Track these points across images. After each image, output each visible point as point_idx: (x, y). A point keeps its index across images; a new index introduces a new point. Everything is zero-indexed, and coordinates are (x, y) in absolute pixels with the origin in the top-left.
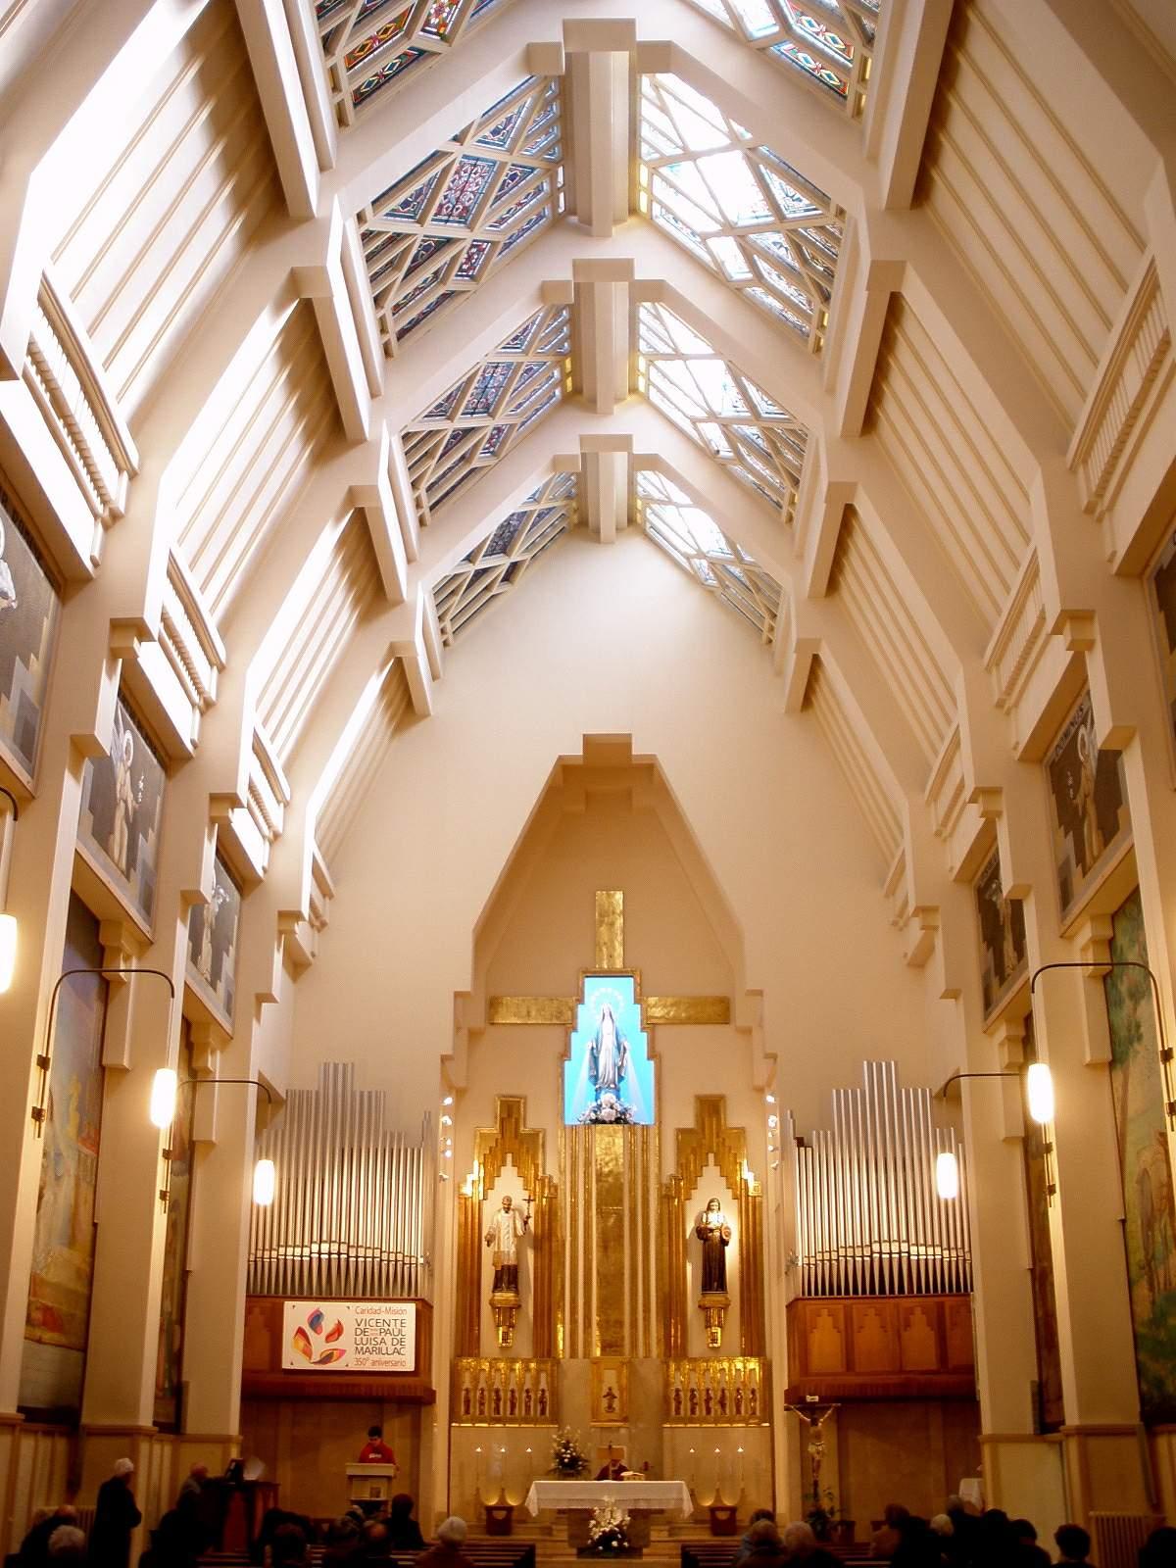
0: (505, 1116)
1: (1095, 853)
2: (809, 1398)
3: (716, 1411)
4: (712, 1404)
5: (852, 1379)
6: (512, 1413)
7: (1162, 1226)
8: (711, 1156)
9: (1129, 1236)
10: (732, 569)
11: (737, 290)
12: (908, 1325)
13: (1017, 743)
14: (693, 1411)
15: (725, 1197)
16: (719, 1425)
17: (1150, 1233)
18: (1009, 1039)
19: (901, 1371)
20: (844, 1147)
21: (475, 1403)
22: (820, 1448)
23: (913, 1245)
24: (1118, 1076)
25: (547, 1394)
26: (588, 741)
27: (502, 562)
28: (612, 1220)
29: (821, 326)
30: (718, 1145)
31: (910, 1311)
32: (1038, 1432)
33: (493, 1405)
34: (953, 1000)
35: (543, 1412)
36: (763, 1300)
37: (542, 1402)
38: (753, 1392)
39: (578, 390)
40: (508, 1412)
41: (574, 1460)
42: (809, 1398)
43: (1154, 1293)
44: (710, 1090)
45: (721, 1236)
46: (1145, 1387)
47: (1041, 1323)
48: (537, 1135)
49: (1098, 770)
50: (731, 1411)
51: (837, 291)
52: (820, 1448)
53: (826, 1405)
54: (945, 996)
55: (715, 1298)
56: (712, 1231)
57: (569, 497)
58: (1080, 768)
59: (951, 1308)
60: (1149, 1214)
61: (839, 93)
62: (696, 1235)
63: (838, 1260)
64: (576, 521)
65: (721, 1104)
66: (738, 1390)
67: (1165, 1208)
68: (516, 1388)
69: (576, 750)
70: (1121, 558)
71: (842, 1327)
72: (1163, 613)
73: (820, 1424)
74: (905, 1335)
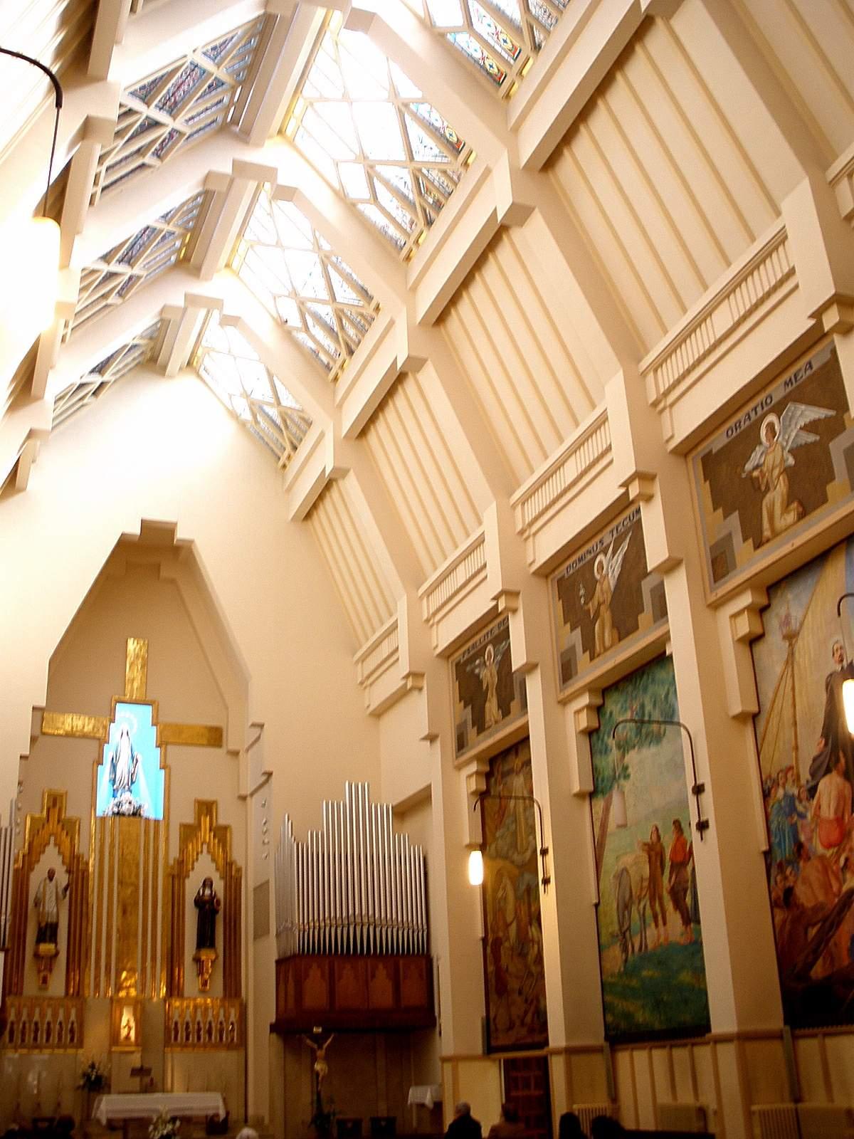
0: (51, 804)
1: (607, 643)
4: (202, 1033)
6: (48, 1040)
7: (642, 906)
9: (601, 917)
10: (267, 409)
11: (351, 207)
12: (373, 976)
14: (187, 1038)
18: (477, 773)
21: (30, 1033)
24: (599, 803)
25: (75, 1025)
26: (145, 524)
27: (97, 379)
28: (129, 891)
29: (417, 242)
33: (32, 1036)
35: (72, 1040)
37: (72, 1031)
39: (187, 259)
40: (44, 1040)
41: (99, 1078)
43: (627, 954)
44: (207, 796)
48: (75, 822)
49: (617, 587)
51: (443, 220)
54: (425, 739)
57: (151, 338)
61: (498, 80)
64: (151, 358)
67: (645, 895)
68: (201, 1020)
69: (135, 530)
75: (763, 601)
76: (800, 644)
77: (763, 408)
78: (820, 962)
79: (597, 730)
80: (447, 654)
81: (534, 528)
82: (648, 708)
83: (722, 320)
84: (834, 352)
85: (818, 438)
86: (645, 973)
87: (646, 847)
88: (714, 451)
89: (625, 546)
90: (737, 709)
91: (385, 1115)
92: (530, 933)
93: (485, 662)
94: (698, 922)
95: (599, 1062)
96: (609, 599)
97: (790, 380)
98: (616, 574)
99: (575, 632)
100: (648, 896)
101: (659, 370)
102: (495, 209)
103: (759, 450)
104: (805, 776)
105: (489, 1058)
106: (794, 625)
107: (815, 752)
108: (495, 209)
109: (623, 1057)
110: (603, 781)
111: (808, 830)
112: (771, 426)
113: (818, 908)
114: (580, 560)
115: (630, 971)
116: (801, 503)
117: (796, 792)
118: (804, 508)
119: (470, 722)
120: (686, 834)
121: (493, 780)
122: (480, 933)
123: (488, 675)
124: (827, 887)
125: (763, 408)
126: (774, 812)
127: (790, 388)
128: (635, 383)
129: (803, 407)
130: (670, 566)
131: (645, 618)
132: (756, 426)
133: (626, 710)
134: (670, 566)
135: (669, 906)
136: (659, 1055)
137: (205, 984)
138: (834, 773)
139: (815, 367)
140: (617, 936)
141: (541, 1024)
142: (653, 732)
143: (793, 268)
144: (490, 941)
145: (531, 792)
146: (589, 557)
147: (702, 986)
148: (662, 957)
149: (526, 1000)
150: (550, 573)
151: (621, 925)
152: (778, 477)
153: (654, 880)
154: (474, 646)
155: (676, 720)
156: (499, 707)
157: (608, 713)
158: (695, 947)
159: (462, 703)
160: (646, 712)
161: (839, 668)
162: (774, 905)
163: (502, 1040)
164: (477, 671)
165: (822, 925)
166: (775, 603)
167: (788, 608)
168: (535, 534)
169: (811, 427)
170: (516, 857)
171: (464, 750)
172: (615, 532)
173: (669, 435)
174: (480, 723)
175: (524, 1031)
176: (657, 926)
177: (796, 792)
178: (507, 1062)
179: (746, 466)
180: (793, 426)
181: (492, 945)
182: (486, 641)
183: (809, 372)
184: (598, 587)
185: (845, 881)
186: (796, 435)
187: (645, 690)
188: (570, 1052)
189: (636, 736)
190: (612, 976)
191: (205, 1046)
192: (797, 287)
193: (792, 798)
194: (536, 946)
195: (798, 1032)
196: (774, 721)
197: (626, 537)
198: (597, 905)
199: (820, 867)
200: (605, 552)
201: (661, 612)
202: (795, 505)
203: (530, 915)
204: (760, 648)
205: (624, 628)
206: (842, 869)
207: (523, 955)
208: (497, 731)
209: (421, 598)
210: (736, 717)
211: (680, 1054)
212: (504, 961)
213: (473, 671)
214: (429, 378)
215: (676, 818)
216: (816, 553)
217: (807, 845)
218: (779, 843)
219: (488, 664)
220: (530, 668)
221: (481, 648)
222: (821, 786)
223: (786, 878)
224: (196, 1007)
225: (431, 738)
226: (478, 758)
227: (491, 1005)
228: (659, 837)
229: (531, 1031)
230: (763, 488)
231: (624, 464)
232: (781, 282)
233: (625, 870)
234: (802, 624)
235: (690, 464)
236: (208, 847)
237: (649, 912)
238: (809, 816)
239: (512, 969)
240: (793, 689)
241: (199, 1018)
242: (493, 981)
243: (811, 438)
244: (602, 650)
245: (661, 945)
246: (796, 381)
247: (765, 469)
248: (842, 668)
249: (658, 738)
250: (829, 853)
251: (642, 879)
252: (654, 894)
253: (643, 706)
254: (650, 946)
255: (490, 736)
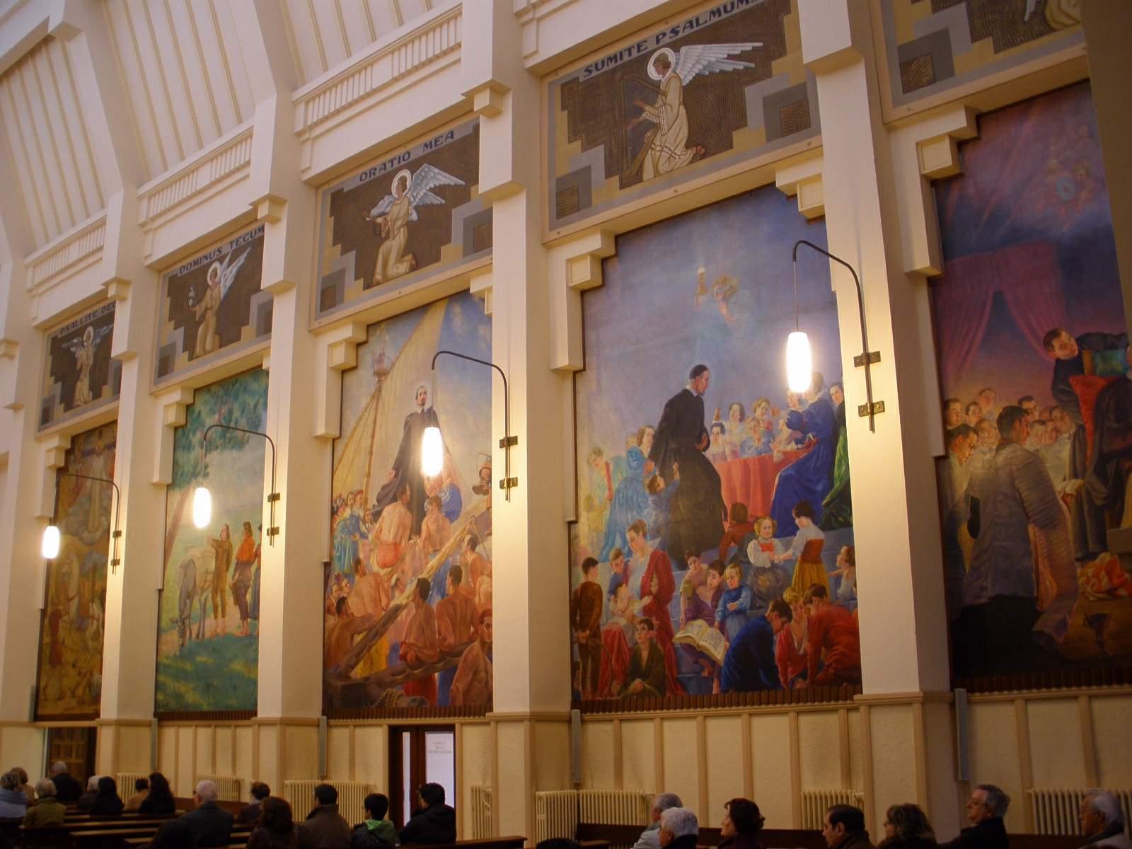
1: (208, 347)
7: (203, 598)
13: (150, 255)
17: (188, 601)
18: (58, 448)
46: (161, 697)
47: (47, 652)
49: (227, 296)
58: (206, 289)
60: (190, 589)
69: (988, 43)
70: (314, 174)
72: (333, 218)
75: (362, 338)
76: (388, 383)
77: (399, 162)
78: (361, 664)
79: (183, 427)
80: (44, 327)
81: (157, 224)
82: (236, 414)
83: (382, 72)
84: (476, 129)
85: (443, 202)
86: (199, 659)
87: (215, 545)
88: (345, 191)
89: (241, 260)
90: (321, 430)
92: (91, 609)
93: (83, 342)
94: (256, 618)
95: (145, 734)
96: (217, 306)
97: (431, 143)
98: (229, 283)
99: (177, 331)
100: (210, 589)
101: (311, 103)
103: (387, 199)
104: (373, 501)
106: (386, 364)
107: (385, 481)
109: (169, 733)
110: (182, 475)
111: (367, 548)
112: (403, 180)
113: (366, 618)
114: (196, 263)
115: (185, 654)
116: (415, 257)
117: (362, 515)
118: (417, 263)
120: (255, 537)
121: (72, 458)
122: (40, 604)
123: (84, 355)
124: (376, 601)
125: (399, 162)
126: (339, 528)
127: (429, 150)
128: (286, 110)
129: (437, 171)
130: (283, 288)
131: (248, 331)
132: (389, 178)
133: (214, 413)
134: (283, 288)
135: (230, 600)
136: (204, 733)
138: (399, 502)
139: (457, 137)
140: (177, 622)
141: (96, 699)
142: (236, 437)
143: (459, 45)
145: (111, 475)
146: (205, 262)
147: (252, 676)
148: (218, 646)
149: (80, 673)
150: (163, 270)
151: (182, 611)
152: (399, 228)
153: (219, 575)
154: (74, 324)
155: (260, 431)
156: (91, 389)
157: (197, 412)
158: (251, 639)
159: (53, 378)
160: (234, 419)
161: (419, 411)
162: (327, 611)
163: (48, 709)
164: (73, 349)
165: (367, 634)
166: (372, 340)
167: (383, 349)
168: (156, 229)
169: (439, 190)
170: (86, 535)
171: (48, 424)
172: (234, 244)
173: (308, 165)
174: (68, 401)
175: (74, 702)
176: (216, 617)
177: (362, 515)
178: (51, 730)
179: (372, 212)
180: (423, 186)
181: (51, 618)
182: (88, 321)
183: (449, 140)
184: (209, 292)
185: (393, 597)
186: (425, 194)
187: (236, 398)
188: (120, 724)
189: (221, 437)
190: (167, 658)
192: (459, 61)
193: (358, 518)
194: (95, 622)
195: (332, 722)
196: (352, 448)
197: (244, 251)
198: (160, 591)
199: (373, 583)
200: (221, 260)
201: (266, 328)
202: (409, 257)
203: (93, 592)
204: (350, 378)
205: (227, 336)
206: (392, 588)
207: (81, 629)
208: (86, 411)
209: (27, 267)
210: (317, 438)
211: (224, 734)
212: (62, 634)
213: (68, 349)
214: (80, 50)
215: (247, 521)
216: (420, 304)
217: (364, 562)
218: (340, 557)
219: (85, 344)
220: (129, 356)
221: (81, 328)
222: (384, 513)
223: (341, 589)
225: (15, 408)
226: (62, 434)
228: (228, 535)
229: (81, 702)
230: (383, 235)
231: (258, 184)
232: (445, 53)
233: (192, 561)
234: (393, 365)
235: (320, 198)
237: (210, 604)
238: (371, 537)
239: (68, 642)
240: (375, 422)
242: (48, 653)
243: (438, 200)
244: (202, 352)
245: (217, 634)
246: (436, 145)
247: (389, 219)
248: (423, 410)
249: (240, 445)
250: (383, 572)
251: (207, 572)
252: (217, 589)
253: (231, 412)
254: (208, 634)
255: (77, 415)
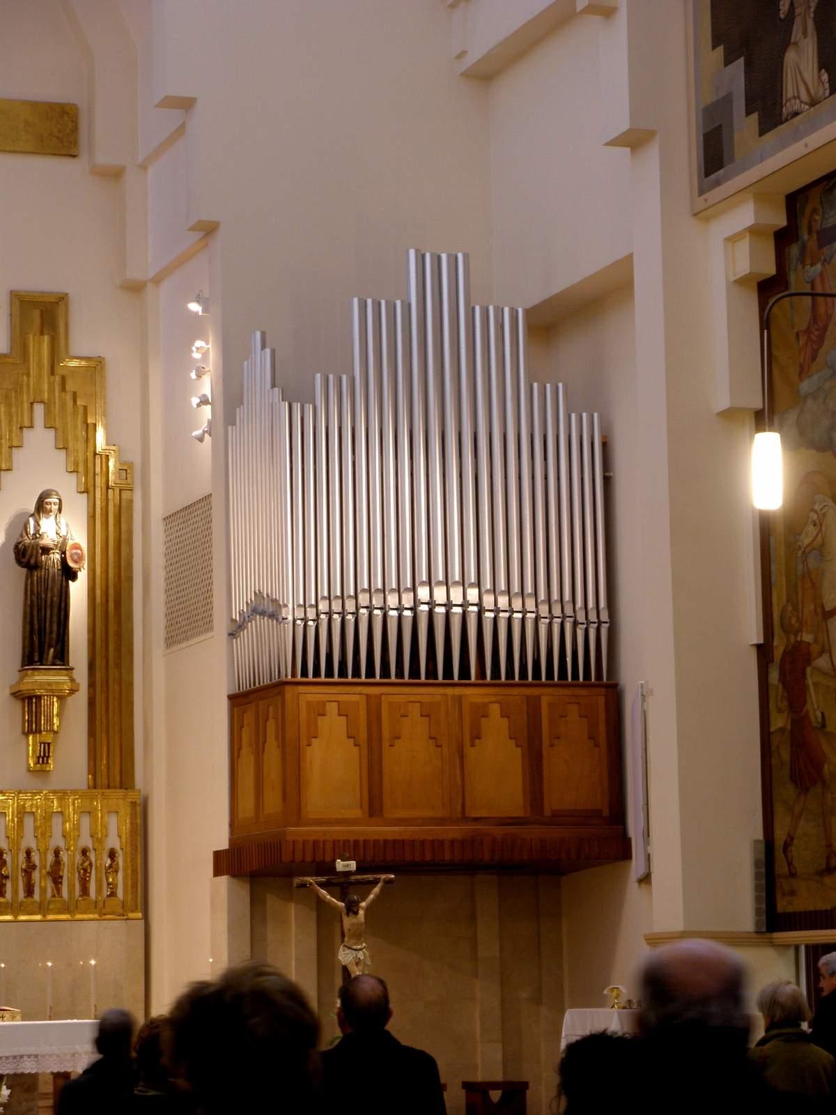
2: (340, 865)
3: (43, 891)
4: (36, 875)
5: (534, 833)
8: (39, 410)
12: (476, 736)
15: (66, 485)
16: (50, 917)
18: (753, 231)
19: (465, 819)
20: (331, 406)
22: (361, 955)
23: (488, 591)
30: (51, 390)
31: (481, 712)
32: (764, 929)
34: (629, 149)
36: (131, 684)
38: (112, 854)
42: (340, 865)
45: (64, 561)
50: (71, 891)
52: (361, 955)
53: (370, 877)
55: (43, 678)
56: (46, 550)
59: (550, 705)
62: (12, 555)
63: (356, 614)
65: (60, 311)
66: (84, 852)
68: (33, 845)
71: (363, 735)
73: (361, 912)
74: (471, 753)
91: (500, 1046)
102: (607, 144)
105: (772, 944)
108: (607, 144)
119: (740, 103)
121: (794, 250)
122: (753, 633)
137: (43, 758)
144: (778, 653)
174: (768, 105)
191: (42, 908)
208: (813, 128)
224: (21, 813)
225: (634, 140)
226: (759, 192)
227: (779, 810)
236: (48, 413)
241: (29, 841)
242: (786, 754)
255: (797, 136)
